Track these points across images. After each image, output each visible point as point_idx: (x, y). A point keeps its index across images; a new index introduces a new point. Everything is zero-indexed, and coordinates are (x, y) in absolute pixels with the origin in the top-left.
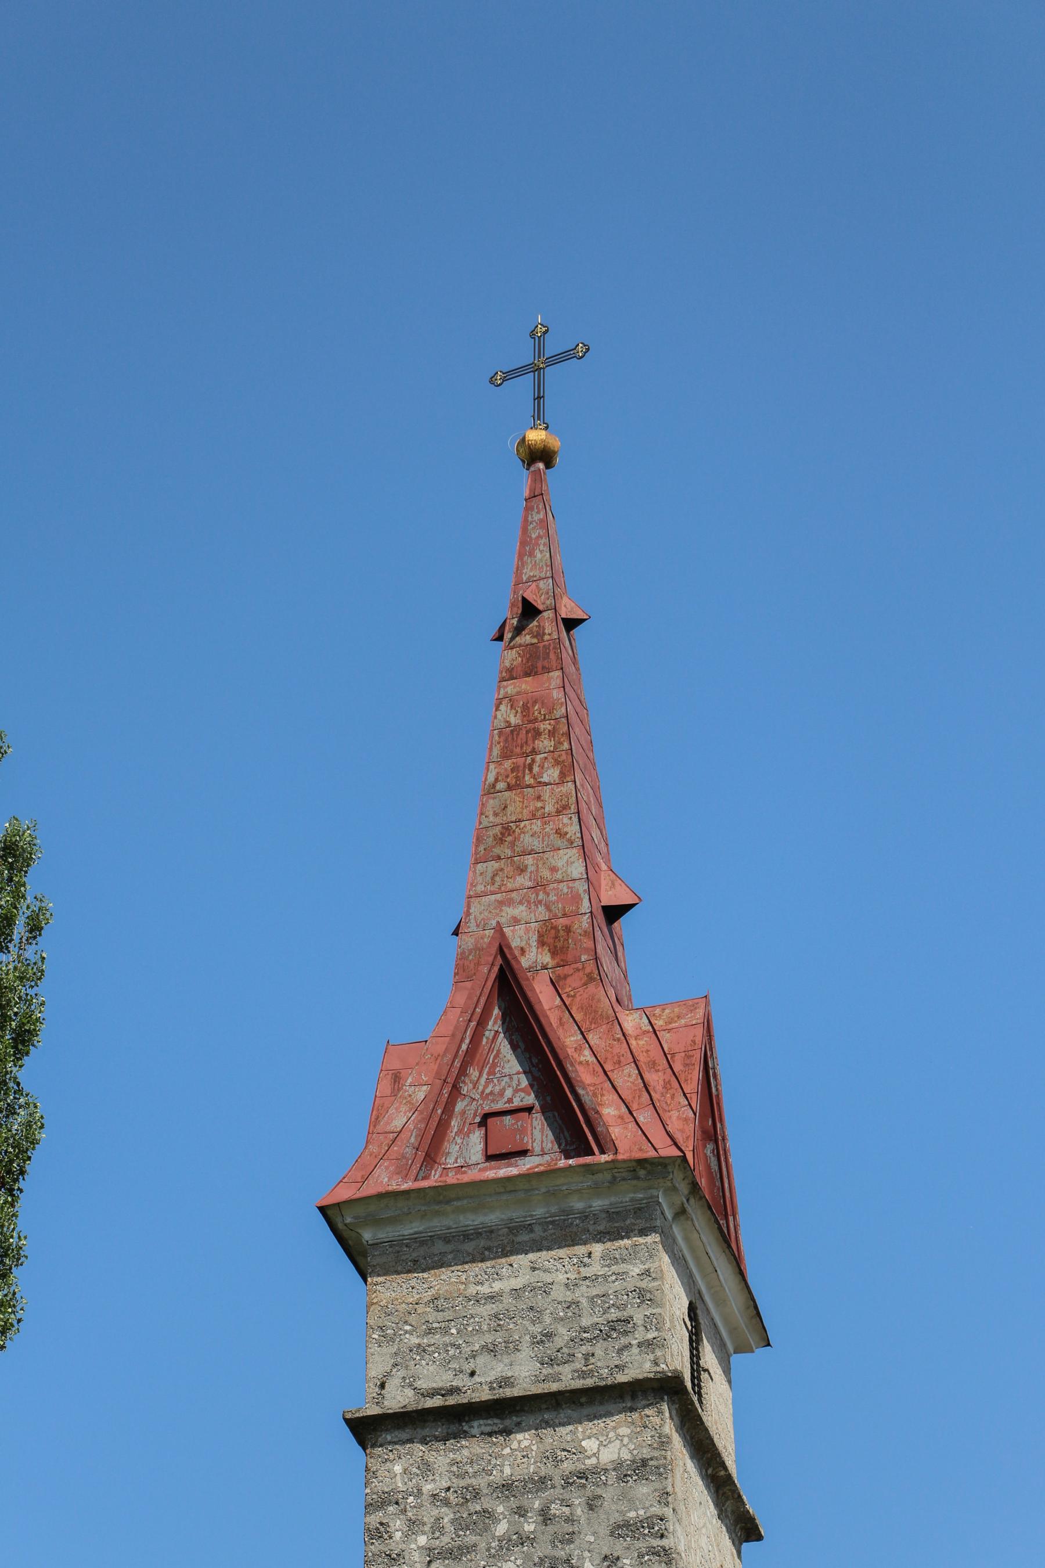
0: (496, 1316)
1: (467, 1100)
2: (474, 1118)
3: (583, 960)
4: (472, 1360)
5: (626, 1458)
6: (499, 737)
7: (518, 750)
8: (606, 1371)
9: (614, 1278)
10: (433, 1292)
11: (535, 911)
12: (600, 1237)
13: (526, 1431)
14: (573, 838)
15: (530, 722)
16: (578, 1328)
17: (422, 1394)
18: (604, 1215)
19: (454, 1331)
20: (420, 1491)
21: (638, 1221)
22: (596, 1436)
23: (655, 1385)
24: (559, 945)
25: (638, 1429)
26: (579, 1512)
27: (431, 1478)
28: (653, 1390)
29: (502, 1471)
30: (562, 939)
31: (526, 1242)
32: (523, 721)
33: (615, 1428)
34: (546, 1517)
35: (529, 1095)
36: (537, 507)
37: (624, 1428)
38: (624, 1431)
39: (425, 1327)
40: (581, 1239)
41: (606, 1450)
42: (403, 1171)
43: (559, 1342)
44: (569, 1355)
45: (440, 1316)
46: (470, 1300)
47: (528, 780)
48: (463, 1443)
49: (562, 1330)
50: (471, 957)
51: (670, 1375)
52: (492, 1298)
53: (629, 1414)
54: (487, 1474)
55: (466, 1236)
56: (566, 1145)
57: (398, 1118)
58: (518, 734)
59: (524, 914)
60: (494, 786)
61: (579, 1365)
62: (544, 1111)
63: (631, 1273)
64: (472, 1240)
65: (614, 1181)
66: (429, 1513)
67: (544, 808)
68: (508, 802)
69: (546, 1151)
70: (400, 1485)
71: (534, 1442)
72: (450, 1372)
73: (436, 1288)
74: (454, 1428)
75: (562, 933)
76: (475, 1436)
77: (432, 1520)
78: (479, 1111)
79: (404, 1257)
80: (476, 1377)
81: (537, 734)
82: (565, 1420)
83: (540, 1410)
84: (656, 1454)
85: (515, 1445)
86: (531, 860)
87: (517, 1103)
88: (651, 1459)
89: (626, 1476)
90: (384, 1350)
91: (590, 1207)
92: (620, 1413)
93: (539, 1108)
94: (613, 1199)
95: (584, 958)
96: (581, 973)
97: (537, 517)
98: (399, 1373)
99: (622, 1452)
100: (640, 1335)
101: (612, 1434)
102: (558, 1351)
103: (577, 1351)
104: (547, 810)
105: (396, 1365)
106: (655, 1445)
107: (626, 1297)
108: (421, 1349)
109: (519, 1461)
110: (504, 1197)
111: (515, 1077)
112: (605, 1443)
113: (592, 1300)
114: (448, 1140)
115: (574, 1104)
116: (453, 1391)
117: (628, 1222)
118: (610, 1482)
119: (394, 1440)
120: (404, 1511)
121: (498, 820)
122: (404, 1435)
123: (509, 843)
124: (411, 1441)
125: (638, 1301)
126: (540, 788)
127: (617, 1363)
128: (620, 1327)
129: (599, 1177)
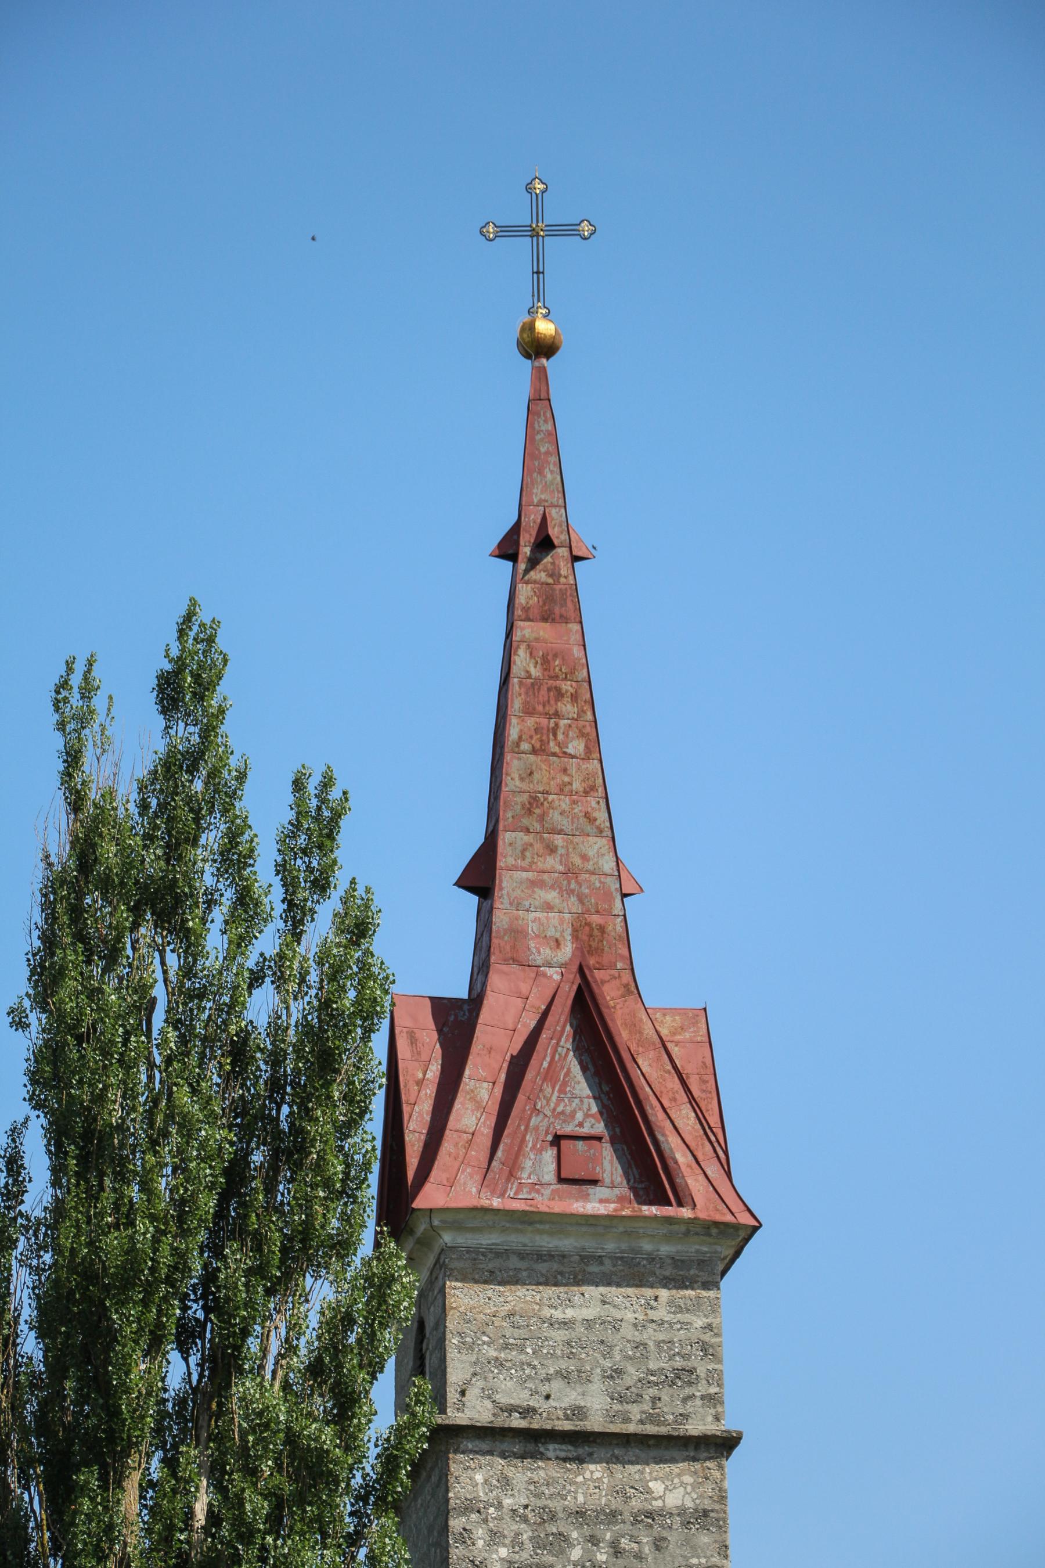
0: (569, 1343)
1: (541, 1116)
2: (546, 1135)
3: (619, 967)
4: (547, 1383)
5: (689, 1505)
6: (520, 688)
7: (540, 708)
8: (671, 1417)
9: (679, 1326)
10: (508, 1307)
11: (567, 901)
12: (667, 1282)
13: (598, 1463)
14: (602, 826)
15: (551, 678)
16: (645, 1370)
17: (501, 1409)
18: (669, 1261)
19: (529, 1350)
20: (500, 1503)
21: (701, 1273)
22: (661, 1479)
23: (719, 1441)
24: (594, 944)
25: (700, 1480)
26: (646, 1550)
27: (510, 1492)
28: (716, 1445)
29: (575, 1498)
30: (596, 939)
31: (596, 1274)
32: (543, 675)
33: (679, 1475)
35: (599, 1123)
36: (544, 414)
37: (687, 1476)
38: (688, 1479)
39: (502, 1341)
40: (648, 1281)
41: (672, 1495)
43: (628, 1381)
44: (637, 1395)
45: (517, 1333)
46: (544, 1322)
47: (553, 747)
48: (540, 1463)
49: (631, 1370)
50: (506, 938)
51: (735, 1435)
52: (565, 1324)
53: (692, 1463)
54: (562, 1498)
55: (540, 1256)
56: (635, 1182)
58: (539, 689)
59: (557, 901)
60: (518, 745)
61: (647, 1407)
62: (613, 1142)
63: (696, 1325)
64: (545, 1261)
65: (687, 1233)
66: (509, 1527)
67: (572, 785)
68: (534, 768)
69: (616, 1184)
70: (481, 1494)
71: (605, 1475)
72: (526, 1391)
73: (512, 1304)
74: (530, 1447)
75: (596, 932)
76: (550, 1459)
77: (512, 1534)
78: (551, 1129)
79: (481, 1266)
80: (551, 1401)
81: (560, 694)
82: (634, 1459)
83: (610, 1444)
84: (717, 1507)
85: (588, 1475)
86: (560, 841)
87: (586, 1130)
88: (712, 1511)
89: (689, 1522)
90: (465, 1358)
91: (658, 1251)
92: (683, 1461)
93: (608, 1138)
94: (680, 1247)
95: (619, 965)
96: (617, 982)
98: (478, 1383)
99: (685, 1499)
100: (702, 1389)
101: (676, 1481)
102: (627, 1389)
103: (644, 1392)
104: (574, 787)
105: (475, 1374)
106: (715, 1498)
107: (689, 1347)
108: (499, 1363)
109: (591, 1491)
110: (584, 1229)
111: (586, 1100)
112: (670, 1488)
113: (658, 1344)
114: (524, 1155)
115: (652, 1148)
116: (527, 1412)
117: (692, 1272)
118: (675, 1527)
119: (475, 1449)
120: (485, 1521)
121: (524, 786)
122: (485, 1446)
123: (538, 816)
124: (490, 1453)
125: (701, 1354)
126: (566, 760)
127: (681, 1411)
128: (686, 1377)
129: (675, 1227)
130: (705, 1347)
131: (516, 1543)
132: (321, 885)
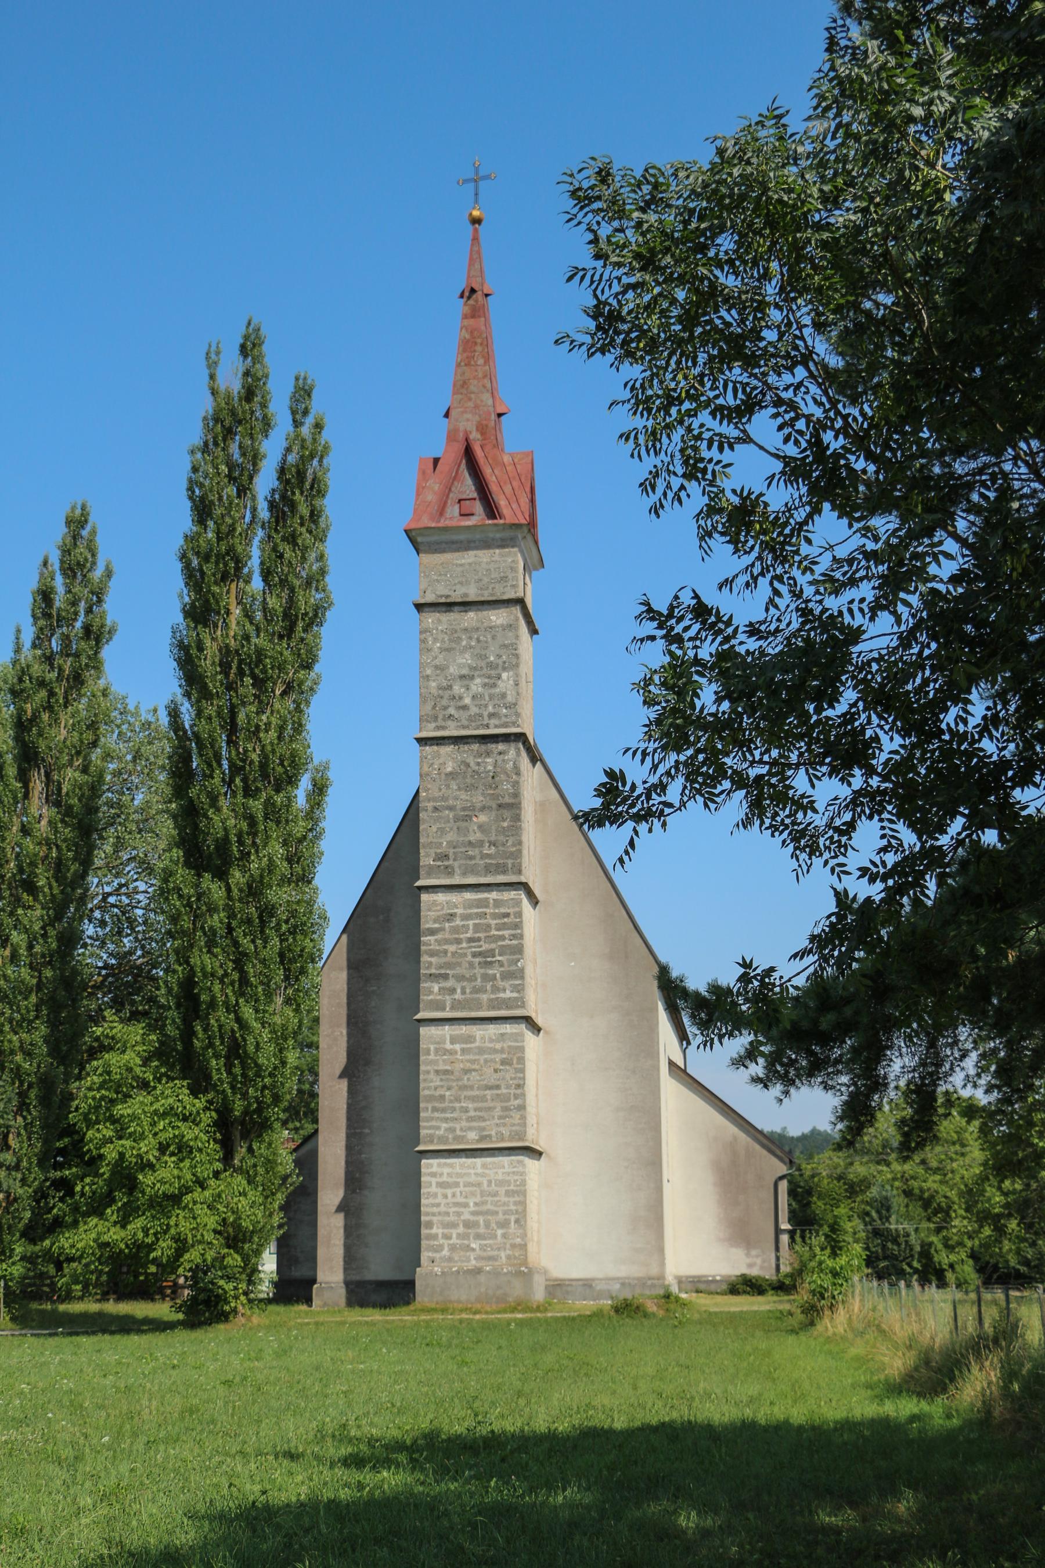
34: (478, 641)
42: (432, 519)
55: (453, 542)
57: (430, 497)
66: (441, 636)
97: (475, 249)
116: (447, 597)
130: (512, 568)
131: (443, 641)
132: (306, 412)
